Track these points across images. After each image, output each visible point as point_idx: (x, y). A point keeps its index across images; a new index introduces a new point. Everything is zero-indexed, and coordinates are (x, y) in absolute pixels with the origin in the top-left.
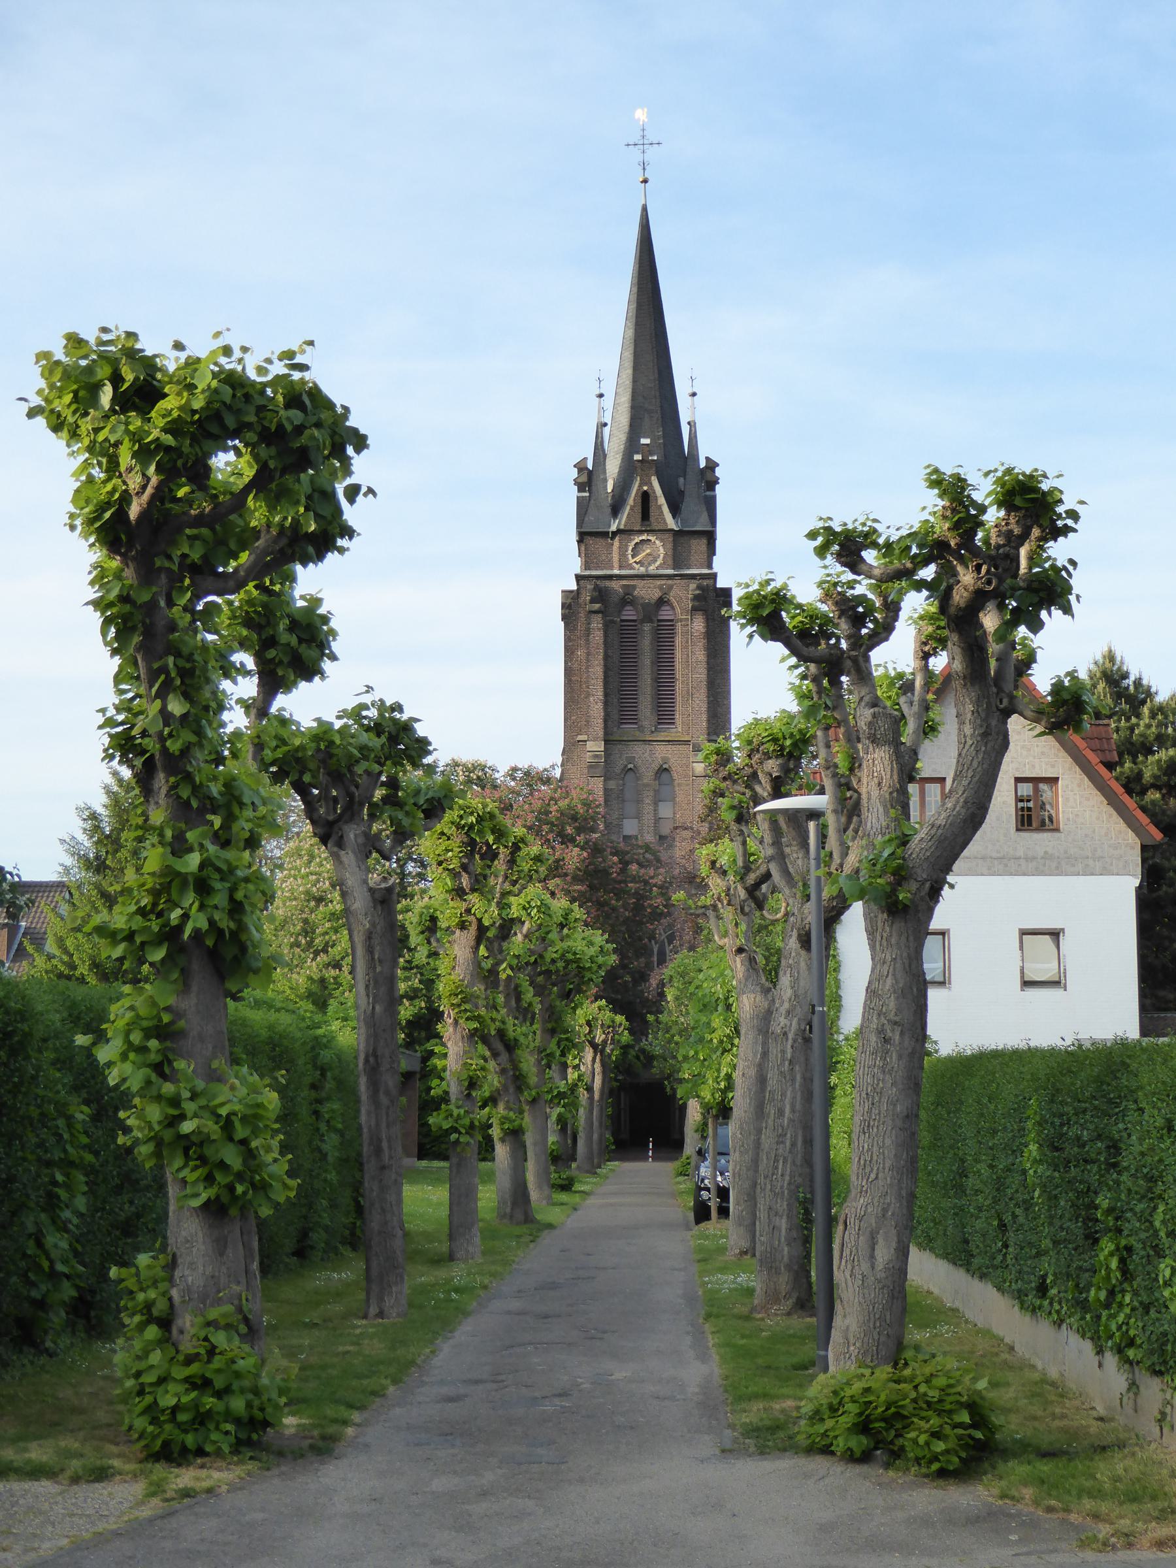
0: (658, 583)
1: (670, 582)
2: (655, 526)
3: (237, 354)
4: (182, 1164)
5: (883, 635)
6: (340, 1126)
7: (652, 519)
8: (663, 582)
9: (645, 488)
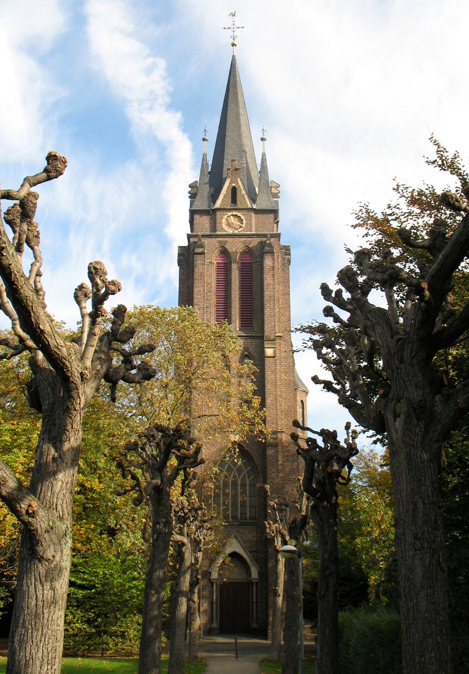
0: (242, 239)
1: (250, 239)
2: (239, 206)
3: (456, 153)
4: (309, 432)
5: (26, 329)
6: (75, 604)
7: (238, 203)
8: (245, 239)
9: (234, 185)
